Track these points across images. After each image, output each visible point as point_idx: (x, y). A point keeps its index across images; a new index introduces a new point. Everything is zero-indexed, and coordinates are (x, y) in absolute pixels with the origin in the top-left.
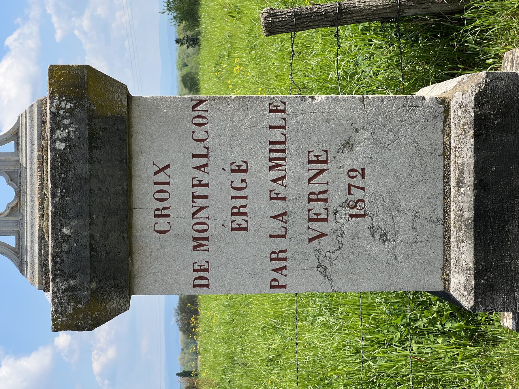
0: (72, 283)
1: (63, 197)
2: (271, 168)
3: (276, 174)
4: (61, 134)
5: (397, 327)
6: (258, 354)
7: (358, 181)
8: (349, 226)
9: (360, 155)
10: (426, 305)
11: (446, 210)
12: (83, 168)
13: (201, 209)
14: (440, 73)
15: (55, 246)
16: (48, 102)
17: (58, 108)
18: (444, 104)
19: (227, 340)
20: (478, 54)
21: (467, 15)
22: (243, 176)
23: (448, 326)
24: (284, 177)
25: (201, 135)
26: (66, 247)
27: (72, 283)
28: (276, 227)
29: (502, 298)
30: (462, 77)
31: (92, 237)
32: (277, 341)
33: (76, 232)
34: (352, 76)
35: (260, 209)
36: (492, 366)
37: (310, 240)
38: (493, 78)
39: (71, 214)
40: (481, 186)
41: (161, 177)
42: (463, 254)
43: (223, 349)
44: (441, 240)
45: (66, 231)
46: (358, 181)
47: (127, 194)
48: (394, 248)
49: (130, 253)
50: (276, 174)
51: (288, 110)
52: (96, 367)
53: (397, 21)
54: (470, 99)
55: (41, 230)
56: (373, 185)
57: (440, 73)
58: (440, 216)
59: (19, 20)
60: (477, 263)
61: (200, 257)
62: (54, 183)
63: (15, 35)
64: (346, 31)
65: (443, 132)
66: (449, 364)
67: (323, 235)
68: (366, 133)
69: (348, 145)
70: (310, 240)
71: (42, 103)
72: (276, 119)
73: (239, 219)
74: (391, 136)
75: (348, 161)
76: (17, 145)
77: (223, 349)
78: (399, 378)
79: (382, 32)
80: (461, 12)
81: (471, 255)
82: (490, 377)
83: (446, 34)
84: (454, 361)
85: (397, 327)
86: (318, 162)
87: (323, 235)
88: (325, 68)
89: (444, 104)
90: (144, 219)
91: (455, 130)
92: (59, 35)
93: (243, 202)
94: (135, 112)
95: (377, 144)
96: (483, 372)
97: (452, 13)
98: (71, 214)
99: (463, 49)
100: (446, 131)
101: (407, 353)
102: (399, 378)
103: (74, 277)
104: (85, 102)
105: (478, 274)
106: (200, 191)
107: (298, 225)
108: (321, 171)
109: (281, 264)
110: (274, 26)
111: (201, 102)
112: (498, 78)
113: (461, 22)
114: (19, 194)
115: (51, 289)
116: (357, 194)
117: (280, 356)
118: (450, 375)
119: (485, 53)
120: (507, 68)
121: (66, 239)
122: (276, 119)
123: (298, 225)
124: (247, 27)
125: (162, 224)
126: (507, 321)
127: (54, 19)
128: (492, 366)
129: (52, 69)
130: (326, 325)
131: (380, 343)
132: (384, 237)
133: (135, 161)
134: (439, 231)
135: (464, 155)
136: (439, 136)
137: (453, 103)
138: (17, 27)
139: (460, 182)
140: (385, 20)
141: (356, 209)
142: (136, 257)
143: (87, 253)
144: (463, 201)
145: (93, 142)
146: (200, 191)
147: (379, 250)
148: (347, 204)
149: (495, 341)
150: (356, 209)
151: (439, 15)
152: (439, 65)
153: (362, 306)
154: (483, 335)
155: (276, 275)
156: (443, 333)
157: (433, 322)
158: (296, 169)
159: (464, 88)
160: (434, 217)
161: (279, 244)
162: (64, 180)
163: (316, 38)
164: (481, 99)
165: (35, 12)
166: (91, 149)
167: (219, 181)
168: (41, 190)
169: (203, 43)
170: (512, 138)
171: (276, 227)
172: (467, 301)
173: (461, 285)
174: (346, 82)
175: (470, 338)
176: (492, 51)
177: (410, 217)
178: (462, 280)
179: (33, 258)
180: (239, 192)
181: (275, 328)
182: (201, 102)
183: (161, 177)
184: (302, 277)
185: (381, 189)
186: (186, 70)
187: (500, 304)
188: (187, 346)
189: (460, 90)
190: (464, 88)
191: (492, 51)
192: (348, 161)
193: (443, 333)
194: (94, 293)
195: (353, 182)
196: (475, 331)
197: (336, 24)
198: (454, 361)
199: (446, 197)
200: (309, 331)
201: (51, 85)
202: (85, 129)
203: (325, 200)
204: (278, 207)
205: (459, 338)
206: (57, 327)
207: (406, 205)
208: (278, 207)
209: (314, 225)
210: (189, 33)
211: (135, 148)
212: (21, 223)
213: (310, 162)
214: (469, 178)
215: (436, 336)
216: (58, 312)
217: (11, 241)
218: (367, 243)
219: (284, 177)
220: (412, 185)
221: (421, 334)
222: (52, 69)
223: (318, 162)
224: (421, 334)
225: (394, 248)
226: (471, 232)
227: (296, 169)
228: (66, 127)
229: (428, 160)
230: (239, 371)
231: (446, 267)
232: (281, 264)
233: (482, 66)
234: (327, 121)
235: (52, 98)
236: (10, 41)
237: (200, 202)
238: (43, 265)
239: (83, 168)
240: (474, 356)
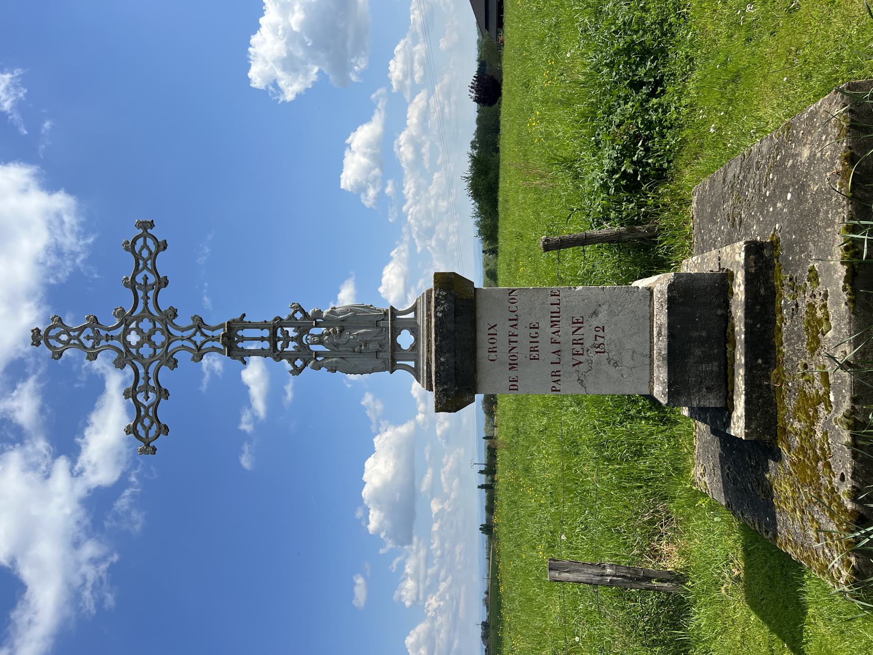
0: (445, 387)
1: (441, 342)
2: (552, 326)
3: (554, 329)
4: (440, 308)
5: (618, 414)
6: (533, 428)
7: (601, 333)
8: (595, 358)
9: (603, 318)
10: (635, 402)
11: (651, 350)
12: (451, 326)
13: (514, 348)
14: (643, 271)
15: (436, 367)
16: (433, 292)
17: (439, 295)
18: (650, 290)
19: (514, 419)
20: (665, 260)
21: (659, 238)
22: (536, 330)
23: (648, 414)
24: (558, 331)
25: (514, 309)
26: (442, 368)
27: (445, 387)
28: (555, 358)
29: (683, 399)
30: (658, 276)
31: (456, 362)
32: (545, 421)
33: (447, 360)
34: (592, 273)
35: (546, 348)
36: (674, 437)
37: (574, 365)
38: (678, 276)
39: (445, 351)
40: (671, 336)
41: (492, 331)
42: (661, 374)
43: (512, 424)
44: (648, 366)
45: (442, 359)
46: (601, 333)
47: (474, 340)
48: (621, 370)
49: (475, 371)
50: (554, 329)
51: (562, 295)
52: (438, 432)
53: (618, 242)
54: (665, 287)
55: (428, 358)
56: (609, 335)
57: (643, 271)
58: (648, 352)
59: (398, 242)
60: (669, 379)
61: (513, 374)
62: (436, 334)
63: (396, 250)
64: (588, 248)
65: (650, 306)
66: (649, 436)
67: (581, 363)
68: (605, 307)
69: (595, 313)
70: (574, 365)
71: (429, 292)
72: (554, 299)
73: (534, 354)
74: (620, 309)
75: (595, 322)
76: (416, 314)
77: (512, 424)
78: (619, 443)
79: (609, 249)
80: (656, 237)
81: (666, 374)
82: (673, 443)
83: (647, 249)
84: (652, 434)
85: (618, 414)
86: (578, 323)
87: (581, 363)
88: (574, 268)
89: (650, 290)
90: (483, 353)
91: (656, 305)
92: (419, 249)
93: (536, 344)
94: (478, 296)
95: (611, 313)
96: (669, 440)
97: (650, 237)
98: (445, 351)
99: (656, 257)
100: (651, 306)
101: (624, 429)
102: (619, 443)
103: (446, 384)
104: (452, 292)
105: (670, 386)
106: (513, 339)
107: (567, 357)
108: (580, 328)
109: (558, 378)
110: (548, 247)
111: (514, 290)
112: (678, 276)
113: (655, 243)
114: (417, 339)
115: (434, 388)
116: (600, 340)
117: (546, 429)
118: (649, 441)
119: (670, 260)
120: (684, 270)
121: (442, 363)
122: (554, 299)
123: (567, 357)
124: (526, 245)
125: (492, 356)
126: (685, 412)
127: (416, 241)
128: (674, 437)
129: (436, 274)
130: (574, 412)
131: (608, 424)
132: (616, 364)
133: (478, 322)
134: (647, 361)
135: (661, 318)
136: (647, 308)
137: (655, 290)
138: (396, 246)
139: (659, 333)
140: (611, 242)
141: (599, 348)
142: (478, 373)
143: (453, 371)
144: (661, 345)
145: (457, 312)
146: (513, 339)
147: (613, 372)
148: (594, 346)
149: (676, 423)
150: (599, 348)
151: (642, 239)
152: (643, 267)
153: (598, 402)
154: (669, 420)
155: (554, 384)
156: (645, 418)
157: (639, 412)
158: (566, 327)
159: (661, 281)
160: (644, 353)
161: (556, 367)
162: (441, 333)
163: (569, 253)
164: (671, 288)
165: (406, 238)
166: (455, 316)
167: (523, 333)
168: (428, 337)
169: (500, 254)
170: (689, 310)
171: (555, 358)
172: (663, 401)
173: (659, 391)
174: (587, 278)
175: (661, 421)
176: (674, 258)
177: (631, 353)
178: (661, 389)
179: (423, 374)
180: (534, 339)
181: (544, 413)
182: (514, 290)
183: (492, 331)
184: (569, 386)
185: (614, 337)
186: (488, 268)
187: (683, 403)
188: (488, 422)
189: (658, 283)
190: (661, 281)
191: (674, 258)
192: (595, 322)
193: (645, 418)
194: (457, 392)
195: (598, 334)
196: (664, 417)
197: (583, 245)
198: (652, 434)
199: (651, 342)
200: (564, 415)
201: (435, 283)
202: (452, 305)
203: (582, 344)
204: (556, 347)
205: (654, 420)
206: (438, 410)
207: (627, 347)
208: (556, 347)
209: (575, 357)
210: (490, 247)
211: (478, 315)
212: (418, 355)
213: (574, 323)
214: (664, 332)
215: (641, 420)
216: (437, 403)
217: (412, 364)
218: (606, 367)
219: (558, 331)
220: (632, 336)
221: (632, 419)
222: (436, 274)
223: (578, 323)
224: (632, 419)
225: (621, 370)
226: (666, 362)
227: (566, 327)
228: (442, 305)
229: (641, 321)
230: (522, 436)
231: (651, 381)
232: (558, 378)
233: (668, 268)
234: (583, 300)
235: (435, 290)
236: (393, 253)
237: (513, 345)
238: (429, 377)
239: (451, 326)
240: (663, 431)
